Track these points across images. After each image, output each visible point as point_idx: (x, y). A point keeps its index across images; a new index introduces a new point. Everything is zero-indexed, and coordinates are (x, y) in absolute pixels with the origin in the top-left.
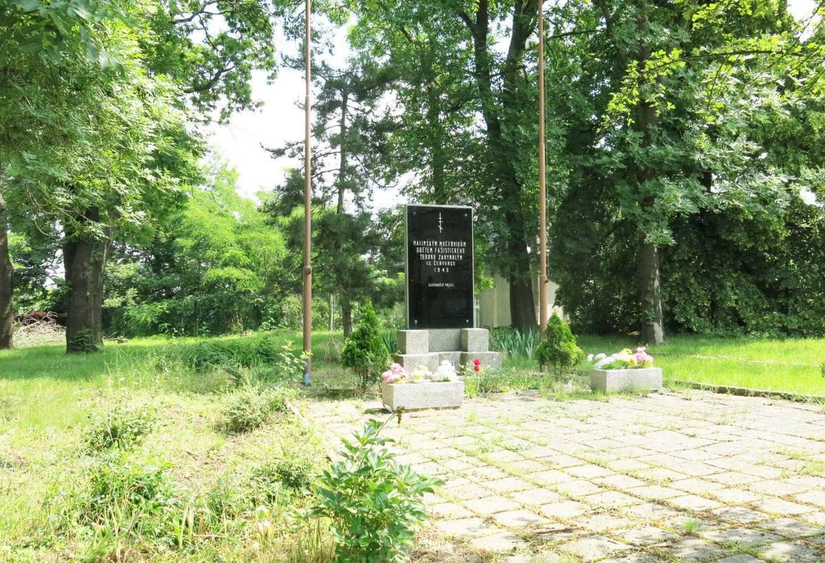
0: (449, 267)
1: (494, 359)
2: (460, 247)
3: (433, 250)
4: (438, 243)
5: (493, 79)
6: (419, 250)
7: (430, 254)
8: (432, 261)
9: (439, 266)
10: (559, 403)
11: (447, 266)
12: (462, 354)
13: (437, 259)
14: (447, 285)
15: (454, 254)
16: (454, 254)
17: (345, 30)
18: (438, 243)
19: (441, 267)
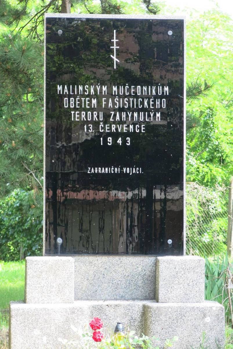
0: (133, 135)
1: (208, 320)
2: (156, 97)
3: (99, 103)
4: (110, 89)
5: (128, 172)
6: (68, 103)
7: (92, 110)
8: (96, 124)
9: (110, 134)
10: (198, 304)
11: (128, 134)
12: (144, 307)
13: (106, 121)
14: (127, 170)
15: (144, 110)
16: (144, 110)
17: (144, 336)
18: (110, 89)
19: (115, 135)
